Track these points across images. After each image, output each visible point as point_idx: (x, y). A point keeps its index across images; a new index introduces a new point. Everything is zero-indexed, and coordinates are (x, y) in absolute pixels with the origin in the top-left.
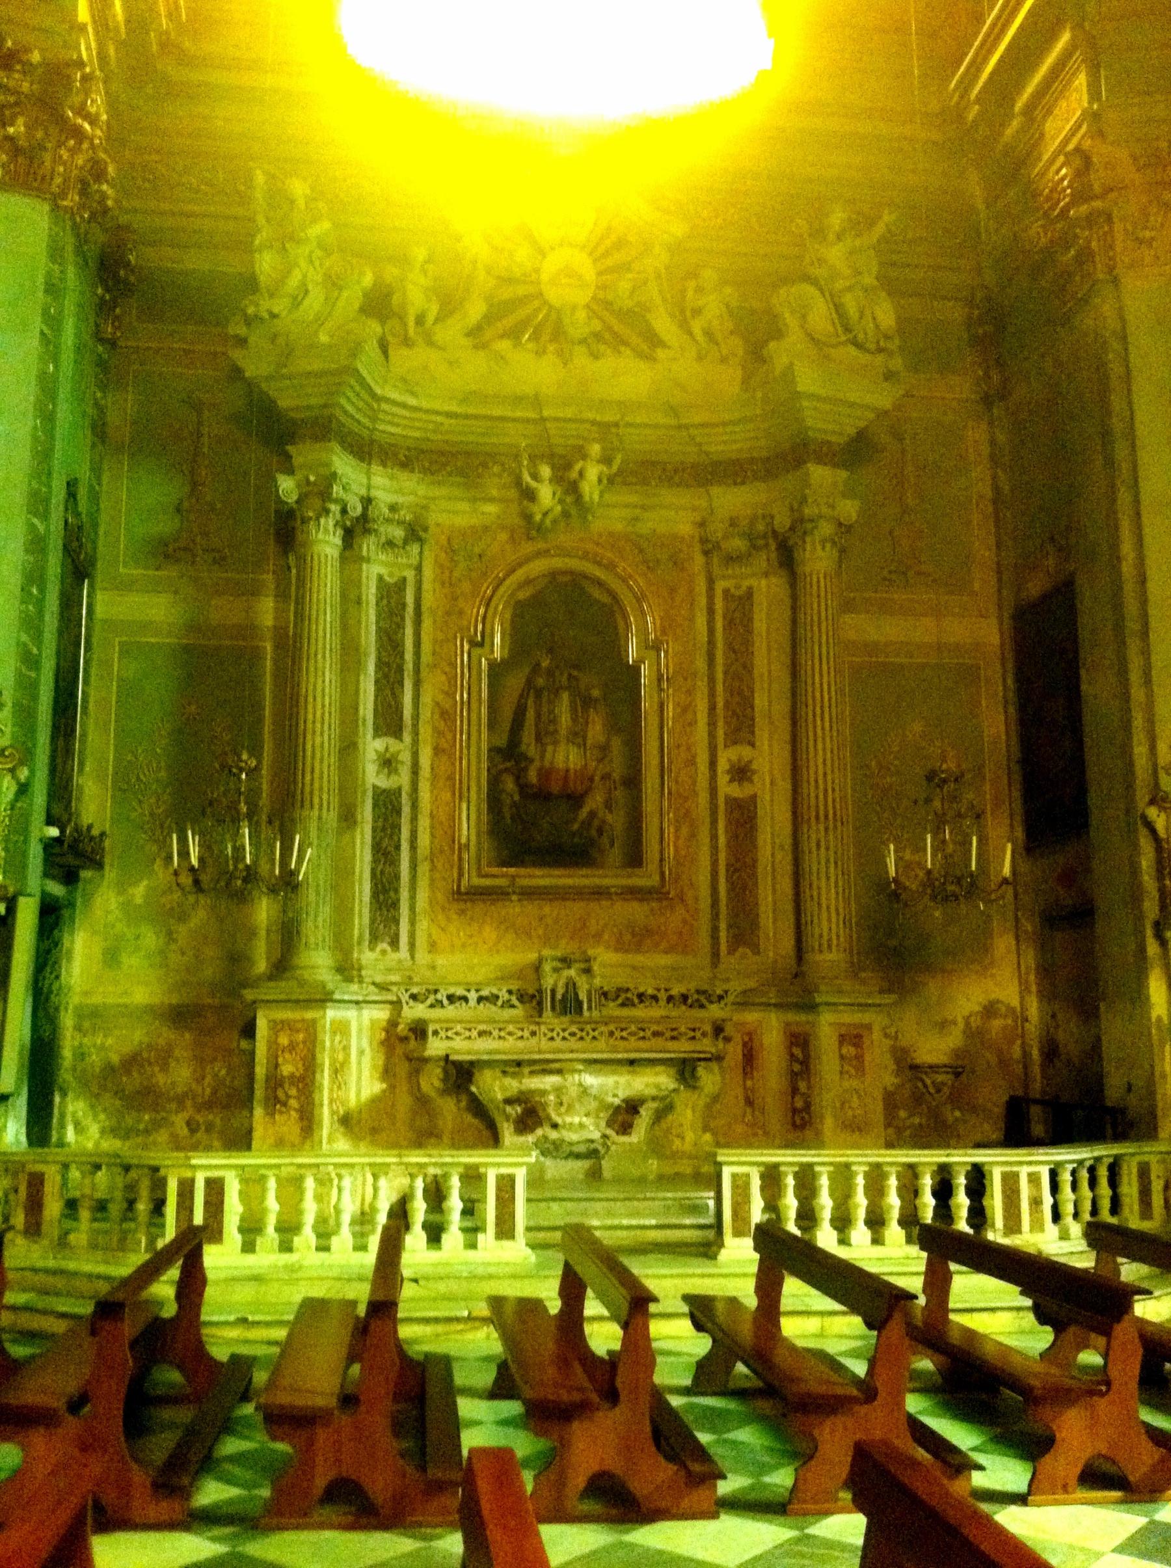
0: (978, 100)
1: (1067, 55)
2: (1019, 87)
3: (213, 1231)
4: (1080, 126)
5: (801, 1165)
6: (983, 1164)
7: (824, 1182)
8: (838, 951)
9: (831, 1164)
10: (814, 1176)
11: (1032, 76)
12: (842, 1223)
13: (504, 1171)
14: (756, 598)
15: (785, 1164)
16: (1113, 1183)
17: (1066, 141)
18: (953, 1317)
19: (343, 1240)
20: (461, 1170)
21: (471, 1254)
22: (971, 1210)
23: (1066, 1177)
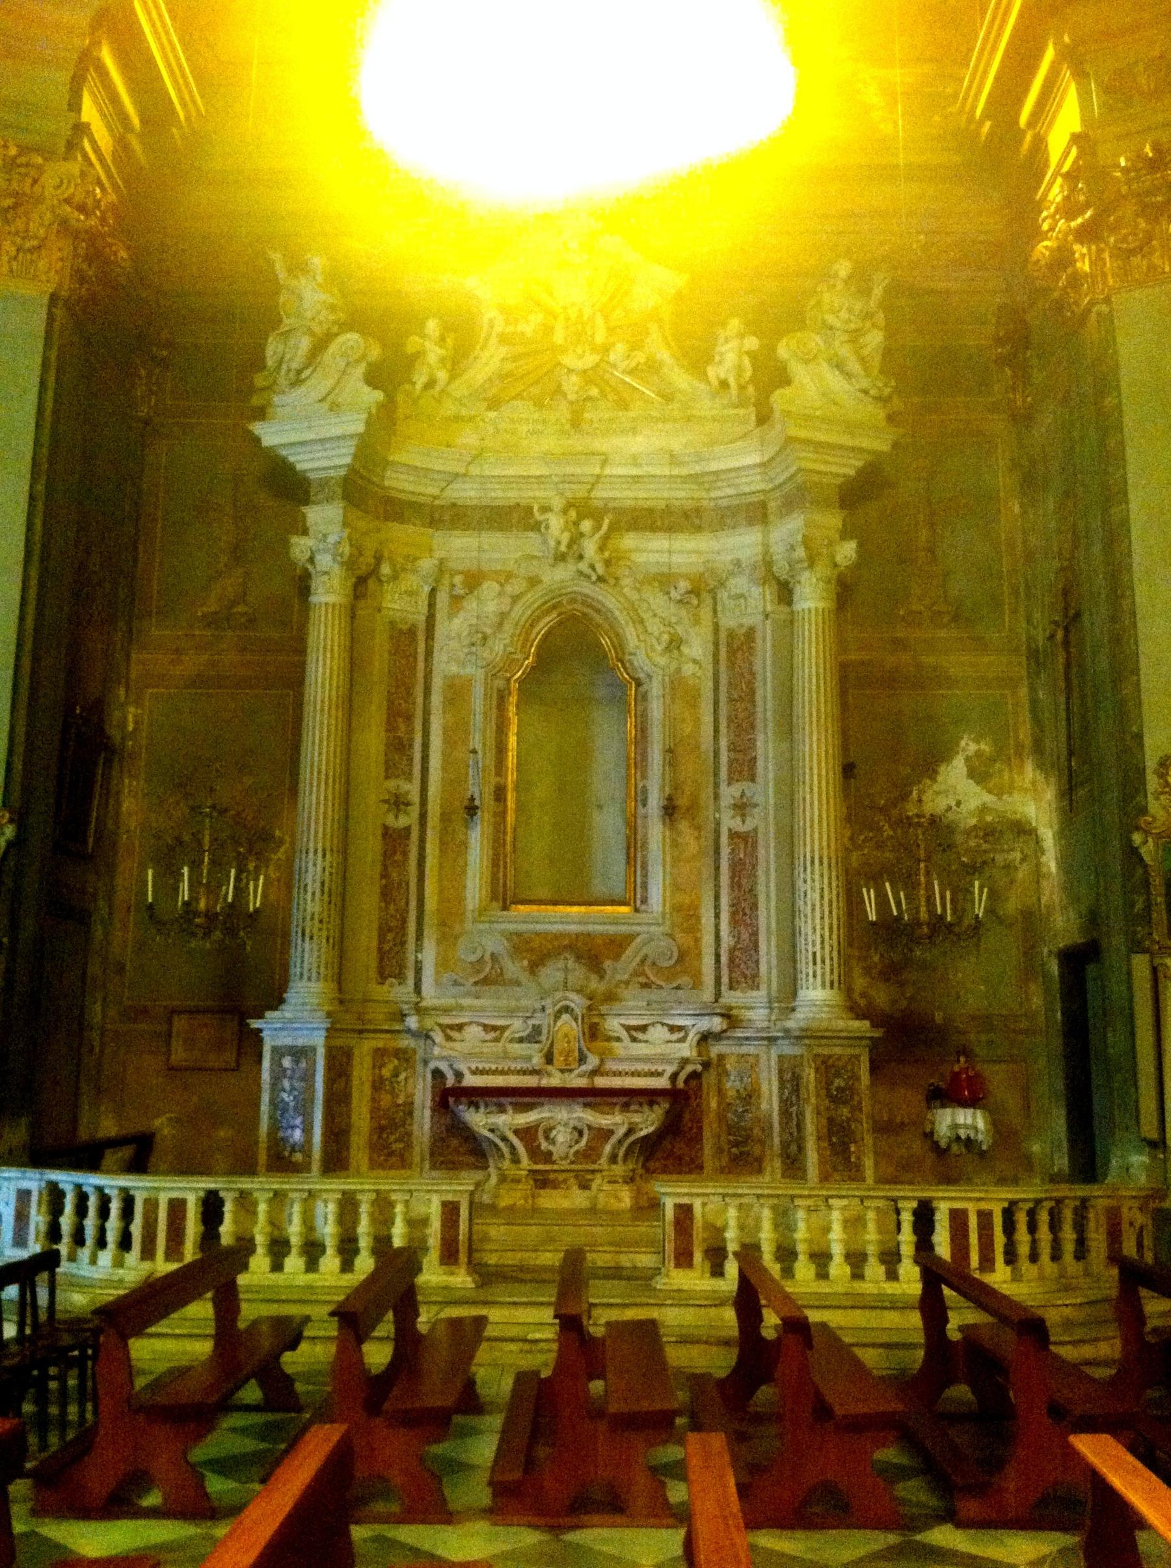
0: (986, 115)
1: (1054, 72)
2: (1020, 101)
3: (245, 1247)
4: (1068, 153)
5: (344, 1193)
6: (355, 1192)
7: (364, 1209)
8: (318, 980)
9: (914, 1198)
10: (221, 1202)
11: (146, 41)
12: (987, 1262)
13: (175, 1195)
14: (759, 635)
15: (362, 1191)
16: (1055, 1226)
17: (1061, 164)
18: (1052, 1348)
19: (330, 1262)
20: (915, 1204)
21: (311, 1277)
22: (1006, 1246)
23: (1022, 1219)
